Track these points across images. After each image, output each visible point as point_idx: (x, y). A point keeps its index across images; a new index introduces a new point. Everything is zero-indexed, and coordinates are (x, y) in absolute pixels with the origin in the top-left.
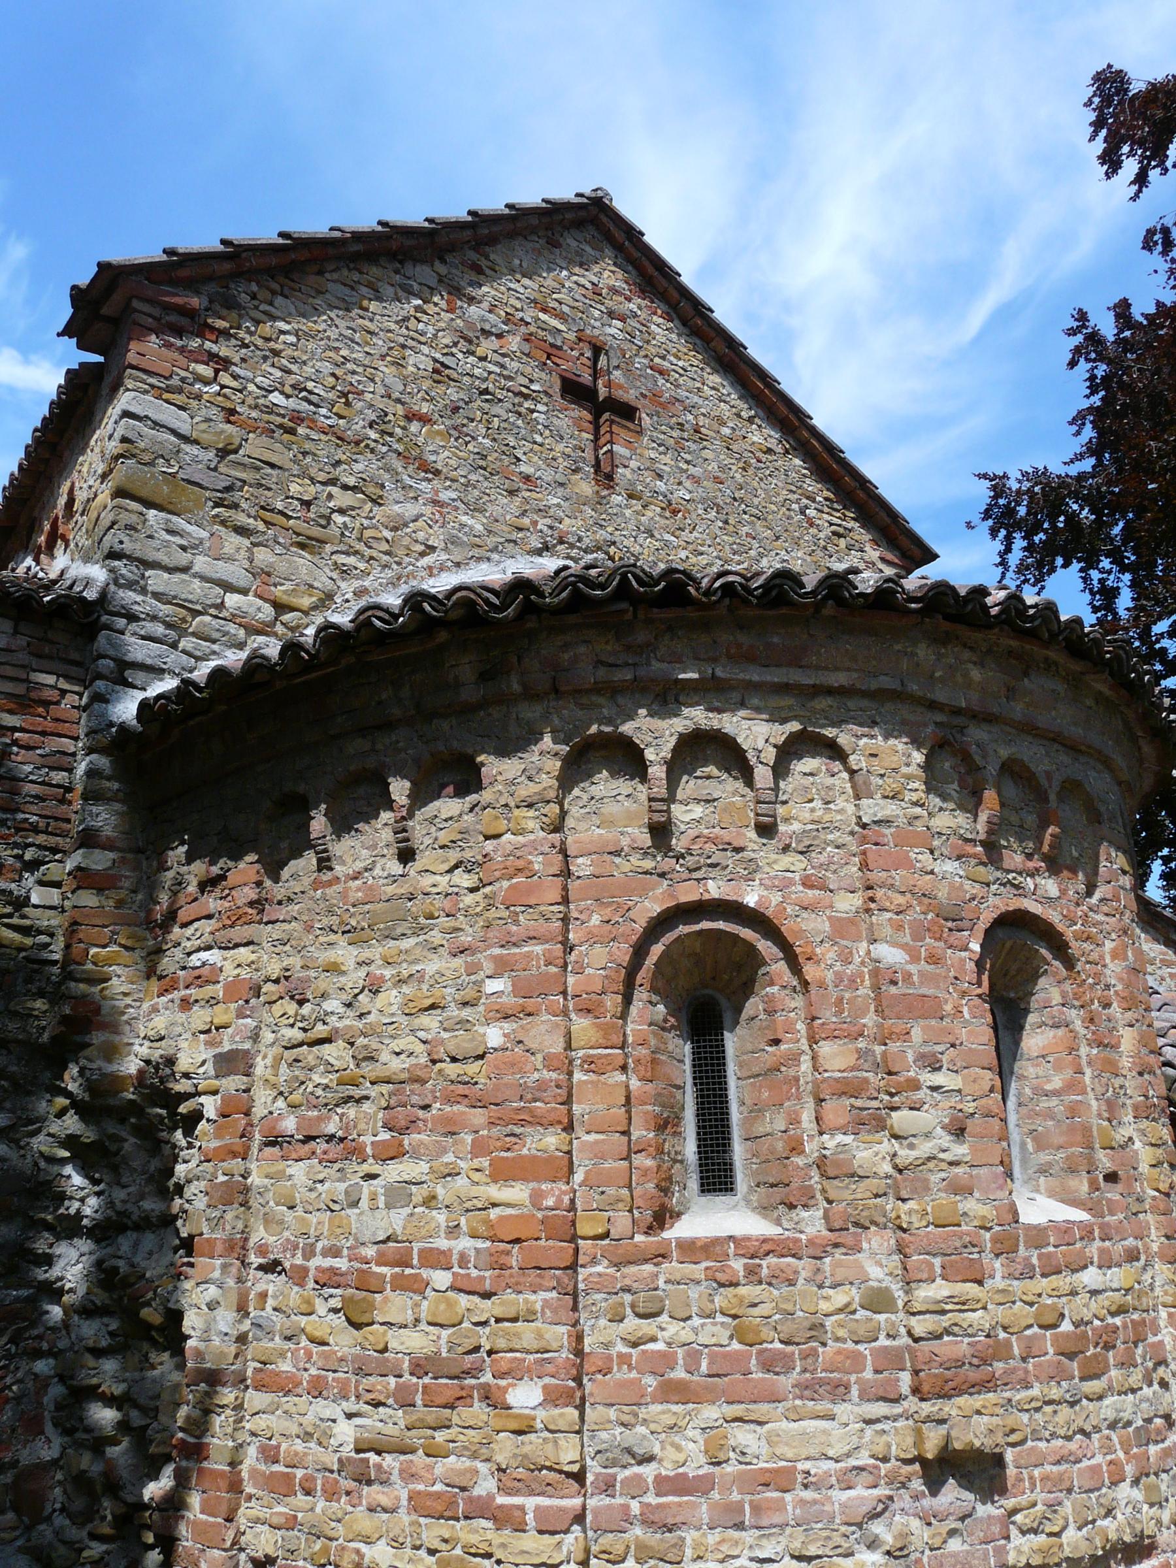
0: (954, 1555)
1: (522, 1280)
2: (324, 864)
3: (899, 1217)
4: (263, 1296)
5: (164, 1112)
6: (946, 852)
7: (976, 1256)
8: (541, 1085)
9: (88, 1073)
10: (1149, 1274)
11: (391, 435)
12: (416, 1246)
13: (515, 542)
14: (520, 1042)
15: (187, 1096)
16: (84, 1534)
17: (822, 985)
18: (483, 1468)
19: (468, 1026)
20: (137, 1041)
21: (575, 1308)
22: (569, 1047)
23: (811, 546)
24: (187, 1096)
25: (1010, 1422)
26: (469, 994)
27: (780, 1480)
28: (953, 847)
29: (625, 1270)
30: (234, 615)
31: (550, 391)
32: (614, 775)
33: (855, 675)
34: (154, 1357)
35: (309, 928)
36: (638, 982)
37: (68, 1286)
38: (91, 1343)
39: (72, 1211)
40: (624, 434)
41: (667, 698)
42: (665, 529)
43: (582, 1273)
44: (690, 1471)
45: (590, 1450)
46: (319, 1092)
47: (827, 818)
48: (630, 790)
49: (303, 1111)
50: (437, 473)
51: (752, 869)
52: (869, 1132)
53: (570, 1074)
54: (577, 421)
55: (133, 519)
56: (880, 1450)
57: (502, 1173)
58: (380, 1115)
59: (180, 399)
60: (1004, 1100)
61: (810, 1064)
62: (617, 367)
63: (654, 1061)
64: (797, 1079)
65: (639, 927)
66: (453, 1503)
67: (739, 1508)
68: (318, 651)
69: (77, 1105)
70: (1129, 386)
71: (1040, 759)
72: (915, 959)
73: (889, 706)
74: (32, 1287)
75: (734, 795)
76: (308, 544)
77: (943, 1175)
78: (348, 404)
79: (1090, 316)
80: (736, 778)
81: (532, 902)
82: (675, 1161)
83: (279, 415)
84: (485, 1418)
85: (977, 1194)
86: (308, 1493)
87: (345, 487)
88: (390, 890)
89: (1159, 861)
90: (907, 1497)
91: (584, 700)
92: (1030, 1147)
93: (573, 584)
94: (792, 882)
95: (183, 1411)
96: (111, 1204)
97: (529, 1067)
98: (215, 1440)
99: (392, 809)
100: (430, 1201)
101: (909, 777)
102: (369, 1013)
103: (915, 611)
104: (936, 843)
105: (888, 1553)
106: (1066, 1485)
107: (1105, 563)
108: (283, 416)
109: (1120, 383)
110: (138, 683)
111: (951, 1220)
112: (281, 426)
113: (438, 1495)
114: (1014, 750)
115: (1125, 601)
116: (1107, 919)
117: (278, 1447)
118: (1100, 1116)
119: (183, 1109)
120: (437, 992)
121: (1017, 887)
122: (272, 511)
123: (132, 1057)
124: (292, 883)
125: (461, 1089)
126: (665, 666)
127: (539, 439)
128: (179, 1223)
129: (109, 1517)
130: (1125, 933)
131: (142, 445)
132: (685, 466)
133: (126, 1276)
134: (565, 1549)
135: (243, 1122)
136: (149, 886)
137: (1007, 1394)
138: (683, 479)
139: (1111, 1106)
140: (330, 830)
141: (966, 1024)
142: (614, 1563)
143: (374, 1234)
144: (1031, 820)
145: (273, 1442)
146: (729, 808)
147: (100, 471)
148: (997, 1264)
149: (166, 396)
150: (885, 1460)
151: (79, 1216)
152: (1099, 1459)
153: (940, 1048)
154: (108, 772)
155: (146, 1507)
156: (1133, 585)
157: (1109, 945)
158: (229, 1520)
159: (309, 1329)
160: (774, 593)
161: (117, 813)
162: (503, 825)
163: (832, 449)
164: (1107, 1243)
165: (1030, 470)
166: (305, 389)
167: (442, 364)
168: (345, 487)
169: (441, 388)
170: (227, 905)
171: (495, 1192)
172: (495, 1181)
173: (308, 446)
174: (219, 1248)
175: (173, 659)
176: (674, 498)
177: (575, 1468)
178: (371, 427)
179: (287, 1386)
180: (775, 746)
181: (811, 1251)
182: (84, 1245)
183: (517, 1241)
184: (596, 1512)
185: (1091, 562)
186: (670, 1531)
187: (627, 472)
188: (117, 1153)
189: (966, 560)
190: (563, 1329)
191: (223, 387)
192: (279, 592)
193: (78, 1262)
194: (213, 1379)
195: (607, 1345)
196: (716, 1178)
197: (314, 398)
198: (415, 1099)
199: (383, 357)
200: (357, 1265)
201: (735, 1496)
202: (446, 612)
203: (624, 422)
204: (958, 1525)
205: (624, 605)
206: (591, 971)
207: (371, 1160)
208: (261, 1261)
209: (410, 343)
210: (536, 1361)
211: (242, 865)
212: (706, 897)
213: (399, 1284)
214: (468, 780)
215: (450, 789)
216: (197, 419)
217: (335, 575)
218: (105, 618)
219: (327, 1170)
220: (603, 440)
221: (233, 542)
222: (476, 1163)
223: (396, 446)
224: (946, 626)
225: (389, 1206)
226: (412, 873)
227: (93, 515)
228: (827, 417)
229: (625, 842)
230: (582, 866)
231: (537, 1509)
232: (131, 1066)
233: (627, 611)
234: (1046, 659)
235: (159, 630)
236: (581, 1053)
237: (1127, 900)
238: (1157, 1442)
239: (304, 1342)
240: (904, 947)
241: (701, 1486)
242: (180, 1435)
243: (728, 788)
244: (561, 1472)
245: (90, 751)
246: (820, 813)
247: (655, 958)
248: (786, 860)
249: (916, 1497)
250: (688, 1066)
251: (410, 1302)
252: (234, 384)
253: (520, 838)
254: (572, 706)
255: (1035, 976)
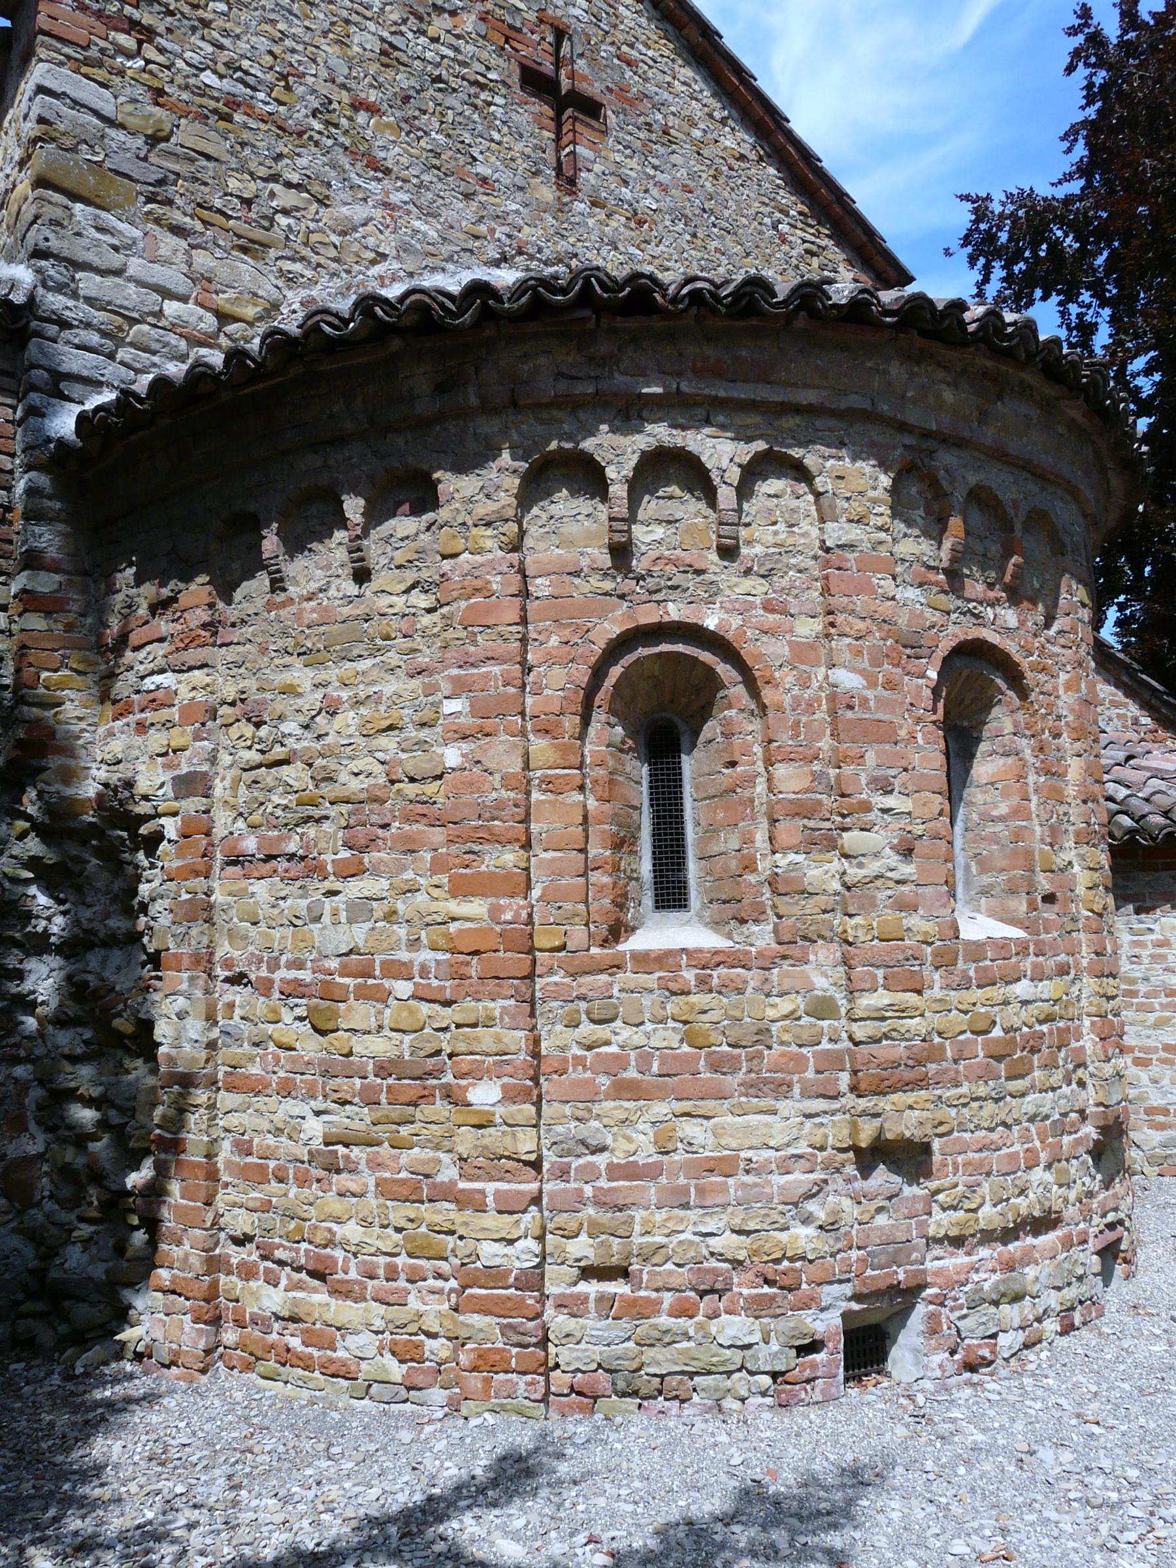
0: (880, 1228)
1: (481, 988)
2: (277, 585)
3: (845, 931)
4: (231, 1006)
5: (125, 834)
6: (908, 579)
7: (917, 968)
8: (500, 805)
9: (46, 796)
10: (1078, 986)
11: (336, 126)
12: (378, 958)
13: (471, 251)
14: (478, 762)
15: (147, 818)
16: (73, 1217)
17: (780, 709)
18: (445, 1158)
19: (426, 747)
20: (94, 765)
21: (532, 1015)
22: (527, 767)
23: (782, 253)
24: (147, 818)
25: (939, 1116)
26: (427, 714)
27: (724, 1166)
28: (916, 574)
29: (581, 980)
30: (173, 325)
31: (509, 81)
32: (574, 493)
33: (824, 393)
34: (128, 1063)
35: (264, 651)
36: (596, 704)
37: (40, 999)
38: (66, 1051)
39: (40, 929)
40: (587, 133)
41: (629, 413)
42: (630, 241)
43: (540, 983)
44: (640, 1159)
45: (546, 1142)
46: (279, 812)
47: (790, 541)
48: (591, 510)
49: (263, 831)
50: (387, 171)
51: (713, 591)
52: (820, 851)
53: (528, 793)
54: (538, 117)
55: (59, 213)
56: (817, 1140)
57: (461, 889)
58: (340, 834)
59: (100, 74)
60: (952, 824)
61: (765, 786)
62: (582, 55)
63: (611, 782)
64: (752, 801)
65: (598, 649)
66: (418, 1188)
67: (685, 1190)
68: (265, 358)
69: (38, 828)
70: (1128, 95)
71: (1007, 487)
72: (872, 684)
73: (858, 427)
74: (5, 999)
75: (696, 516)
76: (250, 248)
77: (889, 893)
78: (288, 88)
79: (1094, 13)
80: (699, 499)
81: (491, 622)
82: (631, 879)
83: (212, 98)
84: (447, 1114)
85: (921, 912)
86: (281, 1181)
87: (289, 185)
88: (346, 611)
89: (1115, 608)
90: (840, 1181)
91: (544, 415)
92: (974, 869)
93: (534, 288)
94: (752, 606)
95: (159, 1111)
96: (77, 922)
97: (487, 787)
98: (190, 1136)
99: (347, 529)
100: (391, 916)
101: (875, 501)
102: (327, 734)
103: (889, 325)
104: (899, 569)
105: (821, 1227)
106: (986, 1169)
107: (1086, 296)
108: (217, 100)
109: (1120, 92)
110: (75, 396)
111: (894, 935)
112: (215, 111)
113: (404, 1182)
114: (983, 476)
115: (1102, 338)
116: (1064, 651)
117: (251, 1141)
118: (1042, 841)
119: (144, 830)
120: (394, 713)
121: (977, 616)
122: (210, 209)
123: (90, 781)
124: (245, 605)
125: (420, 809)
126: (627, 379)
127: (496, 136)
128: (145, 940)
129: (96, 1203)
130: (1080, 665)
131: (62, 127)
132: (652, 172)
133: (95, 991)
134: (523, 1226)
135: (204, 842)
136: (98, 608)
137: (938, 1092)
138: (650, 187)
139: (1054, 831)
140: (282, 550)
141: (919, 749)
142: (568, 1238)
143: (337, 947)
144: (995, 549)
145: (246, 1137)
146: (691, 530)
147: (17, 158)
148: (937, 976)
149: (84, 69)
150: (822, 1149)
151: (46, 934)
152: (1017, 1147)
153: (892, 772)
154: (48, 491)
155: (130, 1194)
156: (1113, 321)
157: (1063, 677)
158: (208, 1204)
159: (275, 1036)
160: (744, 302)
161: (61, 534)
162: (460, 544)
163: (808, 156)
164: (1041, 958)
165: (1015, 192)
166: (240, 69)
167: (391, 45)
168: (289, 185)
169: (389, 74)
170: (179, 627)
171: (455, 907)
172: (455, 897)
173: (246, 136)
174: (186, 962)
175: (112, 371)
176: (640, 207)
177: (533, 1157)
178: (314, 116)
179: (256, 1088)
180: (740, 466)
181: (760, 963)
182: (54, 961)
183: (476, 953)
184: (552, 1195)
185: (1070, 296)
186: (620, 1210)
187: (591, 177)
188: (80, 875)
189: (946, 281)
190: (522, 1034)
191: (148, 62)
192: (221, 300)
193: (49, 977)
194: (186, 1081)
195: (563, 1049)
196: (671, 894)
197: (249, 79)
198: (374, 818)
199: (325, 34)
200: (321, 976)
201: (682, 1181)
202: (399, 317)
203: (588, 120)
204: (886, 1203)
205: (586, 313)
206: (550, 692)
207: (332, 878)
208: (227, 973)
209: (355, 18)
210: (495, 1063)
211: (193, 587)
212: (666, 619)
213: (363, 994)
214: (424, 498)
215: (406, 507)
216: (122, 99)
217: (280, 283)
218: (34, 324)
219: (289, 888)
220: (565, 140)
221: (169, 243)
222: (435, 880)
223: (342, 139)
224: (921, 342)
225: (350, 921)
226: (368, 593)
227: (14, 208)
228: (807, 124)
229: (584, 562)
230: (541, 586)
231: (497, 1192)
232: (90, 790)
233: (589, 319)
234: (1022, 382)
235: (94, 339)
236: (539, 773)
237: (1084, 632)
238: (1070, 1133)
239: (272, 1048)
240: (862, 672)
241: (651, 1172)
242: (158, 1131)
243: (690, 509)
244: (519, 1161)
245: (28, 468)
246: (782, 536)
247: (614, 680)
248: (748, 584)
249: (848, 1181)
250: (645, 788)
251: (373, 1010)
252: (160, 59)
253: (478, 557)
254: (531, 421)
255: (988, 706)
